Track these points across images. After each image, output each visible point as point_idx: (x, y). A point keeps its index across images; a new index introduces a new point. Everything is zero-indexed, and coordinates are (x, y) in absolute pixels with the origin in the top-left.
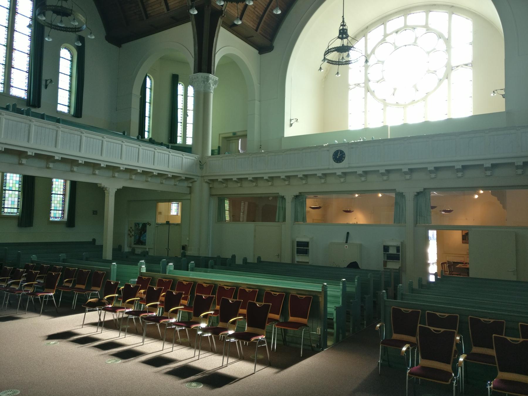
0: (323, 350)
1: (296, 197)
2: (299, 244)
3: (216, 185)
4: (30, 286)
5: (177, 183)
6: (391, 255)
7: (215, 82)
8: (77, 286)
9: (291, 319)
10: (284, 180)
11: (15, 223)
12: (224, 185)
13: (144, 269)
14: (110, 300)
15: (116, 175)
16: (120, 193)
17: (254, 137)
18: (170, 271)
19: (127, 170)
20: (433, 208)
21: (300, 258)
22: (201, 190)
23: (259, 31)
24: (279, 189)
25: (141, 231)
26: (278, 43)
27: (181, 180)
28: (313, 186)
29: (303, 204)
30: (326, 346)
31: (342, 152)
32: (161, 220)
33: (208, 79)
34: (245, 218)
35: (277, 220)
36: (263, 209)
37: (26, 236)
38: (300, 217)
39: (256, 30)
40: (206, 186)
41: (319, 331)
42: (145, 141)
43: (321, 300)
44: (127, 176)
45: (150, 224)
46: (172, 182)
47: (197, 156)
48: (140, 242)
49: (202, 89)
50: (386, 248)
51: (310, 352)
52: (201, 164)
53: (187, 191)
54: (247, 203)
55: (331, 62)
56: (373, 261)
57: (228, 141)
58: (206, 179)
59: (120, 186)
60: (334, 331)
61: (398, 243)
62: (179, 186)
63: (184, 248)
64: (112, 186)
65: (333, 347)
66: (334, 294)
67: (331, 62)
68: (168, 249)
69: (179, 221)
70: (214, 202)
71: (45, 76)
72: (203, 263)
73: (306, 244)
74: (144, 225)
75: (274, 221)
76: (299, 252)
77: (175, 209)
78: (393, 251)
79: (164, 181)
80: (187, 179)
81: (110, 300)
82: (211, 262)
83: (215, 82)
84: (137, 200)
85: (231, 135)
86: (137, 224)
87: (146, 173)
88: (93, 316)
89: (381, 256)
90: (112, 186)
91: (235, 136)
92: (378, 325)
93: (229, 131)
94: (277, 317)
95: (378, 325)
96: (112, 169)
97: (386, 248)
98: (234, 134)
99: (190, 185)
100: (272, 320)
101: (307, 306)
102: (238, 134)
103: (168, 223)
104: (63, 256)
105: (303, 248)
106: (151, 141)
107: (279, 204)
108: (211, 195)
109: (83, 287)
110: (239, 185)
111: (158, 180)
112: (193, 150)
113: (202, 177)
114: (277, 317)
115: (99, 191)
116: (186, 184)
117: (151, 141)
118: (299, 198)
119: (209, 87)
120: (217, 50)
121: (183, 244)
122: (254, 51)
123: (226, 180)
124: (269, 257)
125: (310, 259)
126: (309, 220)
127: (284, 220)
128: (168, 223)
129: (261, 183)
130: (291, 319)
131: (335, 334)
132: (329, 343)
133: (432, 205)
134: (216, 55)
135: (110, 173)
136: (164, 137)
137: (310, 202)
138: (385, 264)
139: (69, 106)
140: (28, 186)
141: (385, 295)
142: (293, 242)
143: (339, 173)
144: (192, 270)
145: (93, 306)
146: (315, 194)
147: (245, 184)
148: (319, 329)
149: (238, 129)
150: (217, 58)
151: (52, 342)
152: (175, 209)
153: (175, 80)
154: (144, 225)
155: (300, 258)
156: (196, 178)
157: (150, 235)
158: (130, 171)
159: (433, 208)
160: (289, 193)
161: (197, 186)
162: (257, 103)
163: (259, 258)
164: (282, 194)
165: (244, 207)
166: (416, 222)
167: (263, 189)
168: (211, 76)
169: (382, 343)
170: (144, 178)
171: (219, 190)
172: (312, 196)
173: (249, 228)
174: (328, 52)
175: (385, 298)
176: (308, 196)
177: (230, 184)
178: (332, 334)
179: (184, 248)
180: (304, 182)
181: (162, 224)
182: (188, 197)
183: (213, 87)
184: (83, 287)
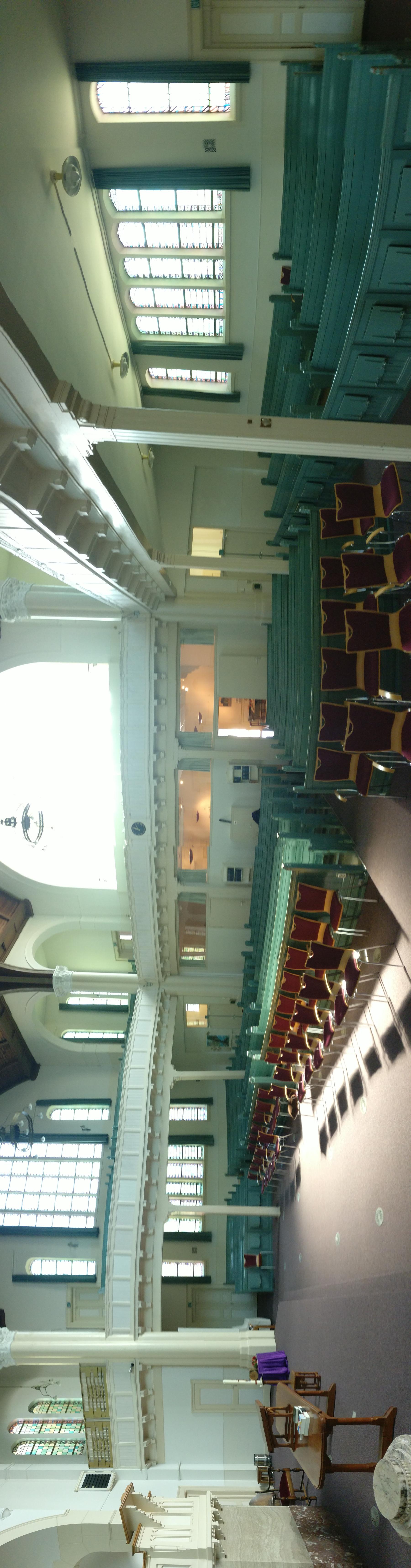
0: (366, 872)
1: (179, 880)
2: (230, 878)
3: (167, 969)
4: (269, 1155)
5: (167, 1010)
6: (243, 775)
7: (62, 969)
8: (272, 1110)
9: (327, 909)
10: (159, 650)
11: (209, 1148)
12: (167, 960)
13: (257, 1057)
14: (290, 1093)
15: (160, 1071)
16: (178, 1065)
17: (116, 922)
18: (259, 1030)
19: (155, 1061)
20: (196, 730)
21: (246, 878)
22: (173, 984)
23: (8, 917)
24: (171, 899)
25: (213, 1040)
26: (21, 896)
27: (164, 1006)
28: (168, 861)
29: (186, 873)
30: (360, 867)
31: (134, 825)
32: (203, 1023)
33: (58, 978)
34: (201, 929)
35: (203, 903)
36: (191, 916)
37: (222, 1141)
38: (201, 877)
39: (8, 920)
40: (170, 980)
41: (341, 876)
42: (103, 1266)
43: (303, 871)
44: (161, 1061)
45: (208, 1033)
46: (166, 1015)
47: (139, 990)
48: (226, 1041)
49: (70, 984)
50: (237, 780)
51: (370, 889)
52: (146, 985)
53: (174, 999)
54: (187, 927)
55: (40, 835)
56: (251, 795)
57: (122, 950)
58: (162, 979)
59: (171, 1067)
60: (337, 853)
61: (231, 767)
62: (169, 1007)
63: (233, 1002)
64: (171, 1075)
65: (362, 856)
66: (295, 853)
67: (40, 835)
68: (233, 1017)
69: (205, 1007)
70: (186, 971)
71: (79, 1131)
72: (252, 993)
73: (230, 871)
74: (209, 1037)
75: (205, 906)
76: (239, 878)
77: (193, 1008)
78: (239, 774)
79: (165, 1025)
80: (162, 1000)
81: (290, 1093)
82: (250, 984)
83: (62, 969)
84: (184, 1048)
85: (116, 948)
86: (208, 1044)
87: (157, 1044)
88: (305, 1107)
89: (245, 786)
90: (171, 1075)
91: (118, 943)
92: (339, 797)
93: (112, 951)
94: (323, 927)
95: (339, 797)
96: (155, 1077)
97: (237, 780)
98: (115, 944)
99: (168, 996)
100: (327, 936)
101: (309, 890)
102: (115, 940)
103: (207, 1017)
104: (240, 1117)
105: (234, 875)
106: (127, 1033)
107: (186, 900)
108: (178, 974)
109: (273, 1107)
110: (166, 945)
111: (164, 1030)
112: (133, 993)
113: (159, 983)
114: (323, 927)
115: (177, 1084)
116: (167, 1001)
117: (127, 1033)
118: (181, 876)
119: (67, 976)
120: (29, 967)
121: (229, 1002)
122: (30, 922)
123: (161, 958)
124: (244, 913)
125: (246, 864)
126: (204, 866)
127: (204, 895)
128: (207, 1017)
129: (164, 920)
130: (327, 909)
131: (342, 852)
132: (355, 861)
133: (193, 730)
134: (35, 968)
135: (159, 1078)
136: (122, 1018)
137: (186, 864)
138: (252, 781)
139: (215, 318)
140: (176, 1139)
141: (299, 787)
142: (227, 885)
143: (156, 829)
144: (260, 1006)
145: (296, 1110)
146: (176, 857)
147: (165, 937)
148: (339, 876)
149: (110, 940)
150: (37, 966)
151: (330, 1149)
152: (193, 1008)
153: (64, 1007)
154: (209, 1037)
155: (246, 878)
156: (161, 991)
157: (220, 1033)
158: (156, 1059)
159: (196, 730)
160: (174, 889)
161: (170, 990)
162: (83, 920)
163: (246, 926)
164: (175, 897)
165: (190, 931)
166: (209, 748)
167: (171, 918)
168: (55, 975)
169: (365, 794)
170: (162, 1045)
171: (173, 967)
172: (179, 860)
173: (211, 932)
174: (27, 838)
175: (303, 788)
176: (179, 866)
177: (166, 954)
178: (341, 856)
179: (233, 1002)
180: (163, 871)
181: (209, 1022)
182: (181, 998)
183: (67, 972)
184: (273, 1107)
